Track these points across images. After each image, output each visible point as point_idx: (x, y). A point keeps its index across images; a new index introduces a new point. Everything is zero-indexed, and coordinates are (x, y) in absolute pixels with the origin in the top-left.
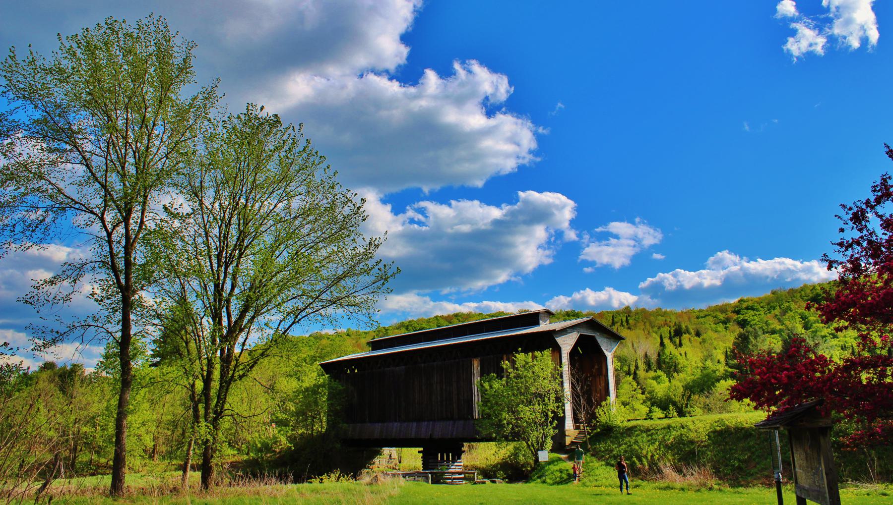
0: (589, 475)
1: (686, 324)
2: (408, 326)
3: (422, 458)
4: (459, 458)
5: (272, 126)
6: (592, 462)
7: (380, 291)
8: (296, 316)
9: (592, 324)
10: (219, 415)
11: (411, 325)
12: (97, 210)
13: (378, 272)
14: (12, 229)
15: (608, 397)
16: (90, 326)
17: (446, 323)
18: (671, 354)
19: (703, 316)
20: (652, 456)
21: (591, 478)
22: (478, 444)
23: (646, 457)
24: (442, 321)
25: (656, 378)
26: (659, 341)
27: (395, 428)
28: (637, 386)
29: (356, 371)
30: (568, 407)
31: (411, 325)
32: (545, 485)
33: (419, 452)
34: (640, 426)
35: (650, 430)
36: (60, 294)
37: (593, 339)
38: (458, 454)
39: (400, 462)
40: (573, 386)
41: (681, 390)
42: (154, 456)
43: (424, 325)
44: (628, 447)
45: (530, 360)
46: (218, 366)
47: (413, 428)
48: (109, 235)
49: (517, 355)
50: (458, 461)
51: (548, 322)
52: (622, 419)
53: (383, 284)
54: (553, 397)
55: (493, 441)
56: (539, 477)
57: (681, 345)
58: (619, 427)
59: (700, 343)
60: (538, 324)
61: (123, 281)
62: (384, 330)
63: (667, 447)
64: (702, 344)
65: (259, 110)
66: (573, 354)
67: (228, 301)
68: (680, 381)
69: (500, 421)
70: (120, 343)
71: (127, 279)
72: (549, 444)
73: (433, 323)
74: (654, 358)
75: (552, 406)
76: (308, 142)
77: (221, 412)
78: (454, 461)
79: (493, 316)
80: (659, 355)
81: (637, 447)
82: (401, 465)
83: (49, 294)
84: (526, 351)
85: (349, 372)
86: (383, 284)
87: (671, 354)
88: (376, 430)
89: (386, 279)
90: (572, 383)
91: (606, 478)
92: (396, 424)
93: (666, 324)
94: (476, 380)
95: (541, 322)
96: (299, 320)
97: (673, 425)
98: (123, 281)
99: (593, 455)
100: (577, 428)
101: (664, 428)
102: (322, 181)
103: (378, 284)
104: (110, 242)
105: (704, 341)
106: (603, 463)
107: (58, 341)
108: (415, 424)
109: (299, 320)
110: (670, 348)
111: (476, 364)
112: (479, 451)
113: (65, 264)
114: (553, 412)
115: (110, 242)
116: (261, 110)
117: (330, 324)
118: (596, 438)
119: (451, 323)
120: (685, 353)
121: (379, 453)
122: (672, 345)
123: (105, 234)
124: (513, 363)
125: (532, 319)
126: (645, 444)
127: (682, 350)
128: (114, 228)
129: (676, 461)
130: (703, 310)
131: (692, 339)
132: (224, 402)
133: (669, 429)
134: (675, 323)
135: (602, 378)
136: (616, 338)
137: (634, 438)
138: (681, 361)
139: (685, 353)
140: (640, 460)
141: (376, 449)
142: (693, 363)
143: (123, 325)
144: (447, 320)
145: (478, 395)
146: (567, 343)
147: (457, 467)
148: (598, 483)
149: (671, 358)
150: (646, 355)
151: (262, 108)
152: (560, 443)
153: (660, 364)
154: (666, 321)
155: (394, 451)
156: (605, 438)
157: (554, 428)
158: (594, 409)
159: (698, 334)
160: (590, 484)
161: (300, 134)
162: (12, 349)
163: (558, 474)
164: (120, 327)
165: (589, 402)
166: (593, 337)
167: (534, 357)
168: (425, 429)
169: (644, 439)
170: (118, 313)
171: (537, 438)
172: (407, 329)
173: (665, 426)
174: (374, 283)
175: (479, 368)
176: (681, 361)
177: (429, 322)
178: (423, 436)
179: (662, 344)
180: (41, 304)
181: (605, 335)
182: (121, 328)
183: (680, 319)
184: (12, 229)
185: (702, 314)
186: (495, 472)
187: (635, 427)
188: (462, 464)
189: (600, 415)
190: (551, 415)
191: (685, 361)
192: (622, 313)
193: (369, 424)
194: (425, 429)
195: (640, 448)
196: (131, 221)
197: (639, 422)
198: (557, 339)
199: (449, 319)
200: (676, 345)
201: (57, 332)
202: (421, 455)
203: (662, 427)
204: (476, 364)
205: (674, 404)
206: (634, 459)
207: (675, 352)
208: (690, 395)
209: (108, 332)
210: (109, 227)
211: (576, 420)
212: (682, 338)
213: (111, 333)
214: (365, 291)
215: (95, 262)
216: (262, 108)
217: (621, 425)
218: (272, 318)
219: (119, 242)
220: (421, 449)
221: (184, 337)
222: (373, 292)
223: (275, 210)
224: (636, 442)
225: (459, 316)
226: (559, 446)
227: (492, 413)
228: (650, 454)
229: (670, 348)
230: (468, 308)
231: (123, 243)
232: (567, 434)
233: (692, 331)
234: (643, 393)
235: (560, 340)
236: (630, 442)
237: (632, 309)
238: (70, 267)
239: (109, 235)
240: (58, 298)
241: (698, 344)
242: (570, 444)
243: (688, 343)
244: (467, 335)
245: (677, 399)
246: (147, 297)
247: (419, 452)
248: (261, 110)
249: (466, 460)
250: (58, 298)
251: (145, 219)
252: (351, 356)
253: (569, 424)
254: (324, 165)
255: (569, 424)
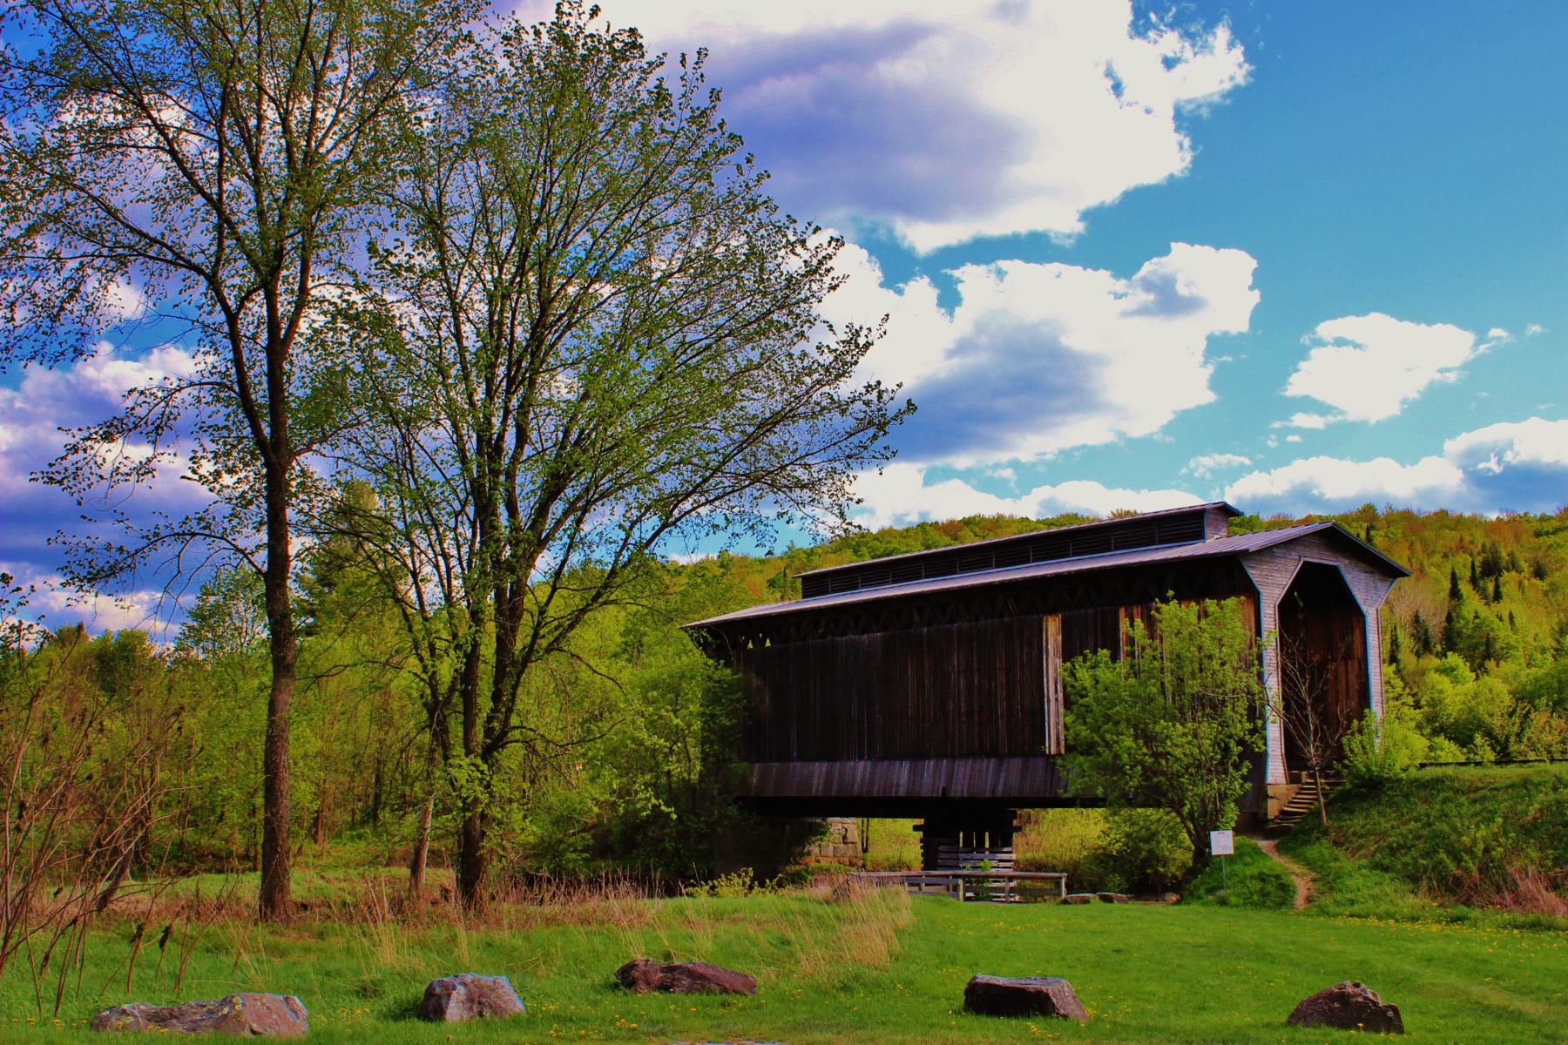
0: (1331, 889)
1: (1509, 549)
2: (858, 545)
3: (921, 841)
4: (1007, 842)
5: (620, 56)
6: (1336, 859)
7: (865, 454)
8: (668, 510)
9: (1332, 536)
10: (496, 741)
11: (865, 544)
12: (198, 259)
13: (864, 408)
14: (9, 315)
15: (1367, 711)
16: (194, 535)
17: (946, 539)
18: (1476, 617)
19: (1551, 530)
20: (1486, 850)
21: (1338, 896)
22: (1042, 812)
23: (1470, 851)
24: (935, 536)
25: (1448, 671)
26: (1447, 585)
27: (860, 773)
28: (1404, 688)
29: (768, 644)
30: (1274, 732)
31: (865, 544)
32: (1224, 910)
33: (916, 828)
34: (1452, 780)
35: (1477, 789)
36: (125, 462)
37: (1334, 572)
38: (1003, 840)
39: (865, 850)
40: (1287, 680)
41: (1507, 700)
42: (316, 832)
43: (895, 544)
44: (1423, 827)
45: (1193, 619)
46: (491, 627)
47: (901, 776)
48: (232, 319)
49: (1164, 607)
50: (1005, 849)
51: (1224, 532)
52: (1407, 762)
53: (875, 437)
54: (1242, 706)
55: (1100, 807)
56: (1210, 891)
57: (1498, 596)
58: (1400, 780)
59: (1546, 594)
60: (1199, 535)
61: (267, 431)
62: (803, 556)
63: (1528, 830)
64: (1551, 594)
65: (586, 17)
66: (1286, 608)
67: (510, 476)
68: (1505, 680)
69: (1117, 756)
70: (264, 575)
71: (276, 425)
72: (1232, 812)
73: (916, 540)
74: (1435, 625)
75: (1240, 727)
76: (715, 95)
77: (504, 733)
78: (995, 848)
79: (1052, 524)
80: (1449, 619)
81: (1446, 828)
82: (868, 855)
83: (100, 461)
84: (1182, 597)
85: (750, 646)
86: (875, 437)
87: (1476, 617)
88: (817, 775)
89: (882, 427)
90: (1284, 671)
91: (1374, 898)
92: (862, 764)
93: (1461, 547)
94: (1054, 666)
95: (1208, 531)
96: (678, 520)
97: (1536, 779)
98: (267, 431)
99: (1336, 843)
100: (1293, 779)
101: (1513, 786)
102: (731, 193)
103: (863, 437)
104: (234, 336)
105: (1554, 588)
106: (1364, 862)
107: (122, 569)
108: (906, 765)
109: (678, 520)
110: (1472, 603)
111: (1053, 628)
112: (1044, 828)
113: (131, 391)
114: (1241, 742)
115: (234, 336)
116: (592, 16)
117: (750, 533)
118: (1343, 802)
119: (956, 539)
120: (1511, 616)
121: (820, 831)
122: (1477, 597)
123: (222, 317)
124: (1151, 624)
125: (1187, 524)
126: (1466, 823)
127: (1504, 607)
128: (241, 306)
129: (1549, 863)
130: (1551, 518)
131: (1526, 583)
132: (510, 711)
133: (1526, 788)
134: (1483, 545)
135: (1354, 666)
136: (1388, 571)
137: (1438, 807)
138: (1502, 632)
139: (1511, 616)
140: (1458, 860)
141: (809, 820)
142: (1530, 639)
143: (271, 534)
144: (946, 533)
145: (1057, 700)
146: (1274, 584)
147: (1002, 864)
148: (1356, 908)
149: (1477, 628)
150: (1416, 619)
151: (595, 11)
152: (1254, 815)
153: (1451, 640)
154: (1461, 540)
155: (852, 825)
156: (1365, 805)
157: (1244, 778)
158: (1341, 736)
159: (1539, 573)
160: (1338, 910)
161: (698, 76)
162: (19, 589)
163: (1257, 885)
164: (263, 537)
165: (1327, 718)
166: (1335, 569)
167: (1203, 614)
168: (931, 777)
169: (1464, 810)
170: (253, 508)
171: (1203, 801)
172: (856, 552)
173: (1516, 780)
174: (851, 435)
175: (1060, 638)
176: (1501, 634)
177: (905, 537)
178: (926, 792)
179: (1455, 593)
180: (84, 485)
181: (1363, 566)
182: (265, 539)
183: (1495, 537)
184: (9, 315)
185: (1548, 527)
186: (1101, 879)
187: (1439, 780)
188: (1014, 856)
189: (1352, 751)
190: (1236, 750)
191: (1510, 633)
192: (1354, 520)
193: (799, 764)
194: (931, 777)
195: (1454, 829)
196: (281, 288)
197: (1450, 771)
198: (1250, 572)
199: (952, 529)
200: (1485, 597)
201: (121, 549)
202: (920, 834)
203: (1509, 782)
204: (1053, 628)
205: (1489, 734)
206: (1443, 855)
207: (1485, 612)
208: (1529, 712)
209: (238, 550)
210: (232, 303)
211: (1294, 758)
212: (1501, 580)
213: (242, 551)
214: (831, 453)
215: (201, 384)
216: (595, 11)
217: (1403, 775)
218: (604, 520)
219: (254, 338)
220: (921, 822)
221: (409, 562)
222: (849, 457)
223: (621, 255)
224: (1444, 815)
225: (977, 524)
226: (1253, 823)
227: (1097, 738)
228: (1481, 846)
229: (1472, 603)
230: (987, 506)
231: (263, 338)
232: (1270, 792)
233: (1524, 565)
234: (1417, 706)
235: (1255, 574)
236: (1428, 815)
237: (1379, 512)
238: (143, 398)
239: (232, 319)
240: (123, 470)
241: (1540, 596)
242: (1276, 817)
243: (1516, 593)
244: (920, 578)
245: (1496, 722)
246: (316, 464)
247: (916, 828)
248: (592, 16)
249: (1021, 849)
250: (123, 470)
251: (310, 284)
252: (753, 609)
253: (1276, 770)
254: (738, 156)
255: (1276, 770)
